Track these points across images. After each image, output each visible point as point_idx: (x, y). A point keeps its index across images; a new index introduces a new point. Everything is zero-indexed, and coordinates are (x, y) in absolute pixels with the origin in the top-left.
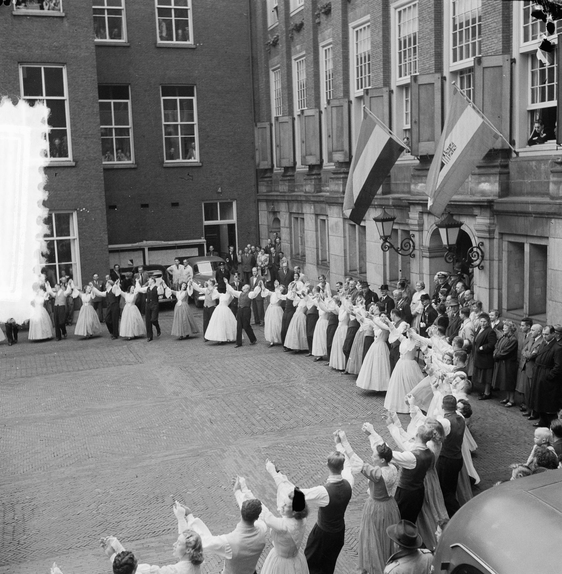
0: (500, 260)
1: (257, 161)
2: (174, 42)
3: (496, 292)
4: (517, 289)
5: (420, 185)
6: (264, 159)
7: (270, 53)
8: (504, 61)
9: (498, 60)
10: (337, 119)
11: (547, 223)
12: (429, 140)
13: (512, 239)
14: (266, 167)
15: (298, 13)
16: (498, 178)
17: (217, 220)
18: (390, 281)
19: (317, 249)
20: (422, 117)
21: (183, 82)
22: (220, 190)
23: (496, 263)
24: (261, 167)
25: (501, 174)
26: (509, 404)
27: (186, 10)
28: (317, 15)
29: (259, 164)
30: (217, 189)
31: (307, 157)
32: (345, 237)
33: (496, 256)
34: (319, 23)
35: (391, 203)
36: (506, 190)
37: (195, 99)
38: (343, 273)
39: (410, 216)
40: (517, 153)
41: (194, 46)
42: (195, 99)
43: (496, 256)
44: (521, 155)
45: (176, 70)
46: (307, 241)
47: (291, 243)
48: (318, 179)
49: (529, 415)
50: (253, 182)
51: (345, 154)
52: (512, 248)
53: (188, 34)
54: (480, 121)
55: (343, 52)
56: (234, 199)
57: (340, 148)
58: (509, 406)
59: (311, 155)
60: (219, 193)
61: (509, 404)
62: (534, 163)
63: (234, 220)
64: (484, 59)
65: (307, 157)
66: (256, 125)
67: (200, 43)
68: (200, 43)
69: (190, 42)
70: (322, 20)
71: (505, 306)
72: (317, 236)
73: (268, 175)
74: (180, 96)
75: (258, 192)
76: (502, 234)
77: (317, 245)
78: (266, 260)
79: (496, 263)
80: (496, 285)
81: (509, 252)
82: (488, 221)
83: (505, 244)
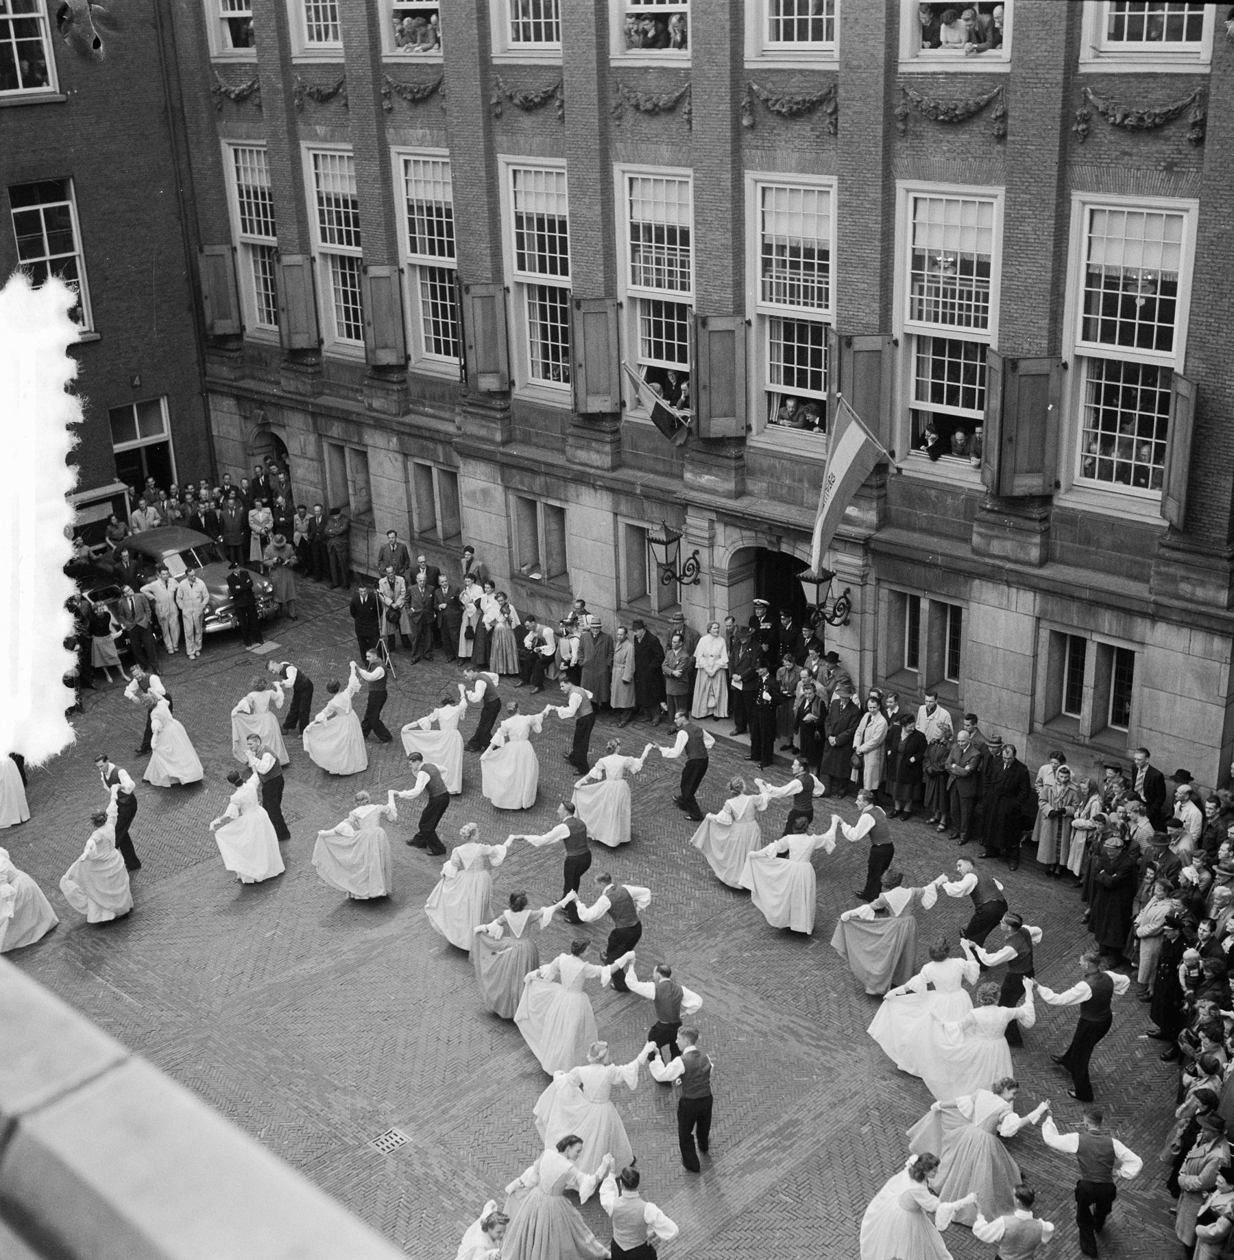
0: (876, 613)
1: (208, 321)
2: (21, 90)
3: (869, 656)
4: (895, 648)
5: (707, 477)
6: (225, 316)
7: (220, 110)
8: (883, 345)
9: (875, 343)
10: (484, 318)
11: (966, 582)
12: (725, 416)
13: (895, 588)
14: (230, 331)
15: (319, 65)
16: (874, 504)
17: (135, 438)
18: (629, 602)
19: (410, 512)
20: (715, 380)
21: (50, 176)
22: (137, 382)
23: (869, 618)
24: (219, 331)
25: (879, 498)
26: (941, 827)
27: (34, 21)
28: (385, 95)
29: (212, 327)
30: (133, 379)
31: (378, 352)
32: (508, 516)
33: (870, 608)
34: (390, 110)
35: (638, 491)
36: (885, 520)
37: (72, 205)
38: (508, 574)
39: (688, 521)
40: (899, 470)
41: (63, 98)
42: (72, 205)
43: (870, 608)
44: (904, 472)
45: (34, 151)
46: (379, 495)
47: (324, 488)
48: (402, 390)
49: (958, 836)
50: (194, 356)
51: (502, 378)
52: (892, 597)
53: (44, 71)
54: (864, 437)
55: (489, 203)
56: (162, 396)
57: (492, 368)
58: (942, 831)
59: (386, 347)
60: (137, 386)
61: (941, 827)
62: (933, 492)
63: (166, 435)
64: (855, 340)
65: (378, 352)
66: (201, 251)
67: (72, 90)
68: (72, 90)
69: (51, 88)
70: (396, 106)
71: (882, 672)
72: (407, 491)
73: (232, 345)
74: (42, 203)
75: (205, 374)
76: (878, 580)
77: (409, 505)
78: (267, 521)
79: (869, 618)
80: (869, 644)
81: (890, 603)
82: (860, 562)
83: (884, 593)
